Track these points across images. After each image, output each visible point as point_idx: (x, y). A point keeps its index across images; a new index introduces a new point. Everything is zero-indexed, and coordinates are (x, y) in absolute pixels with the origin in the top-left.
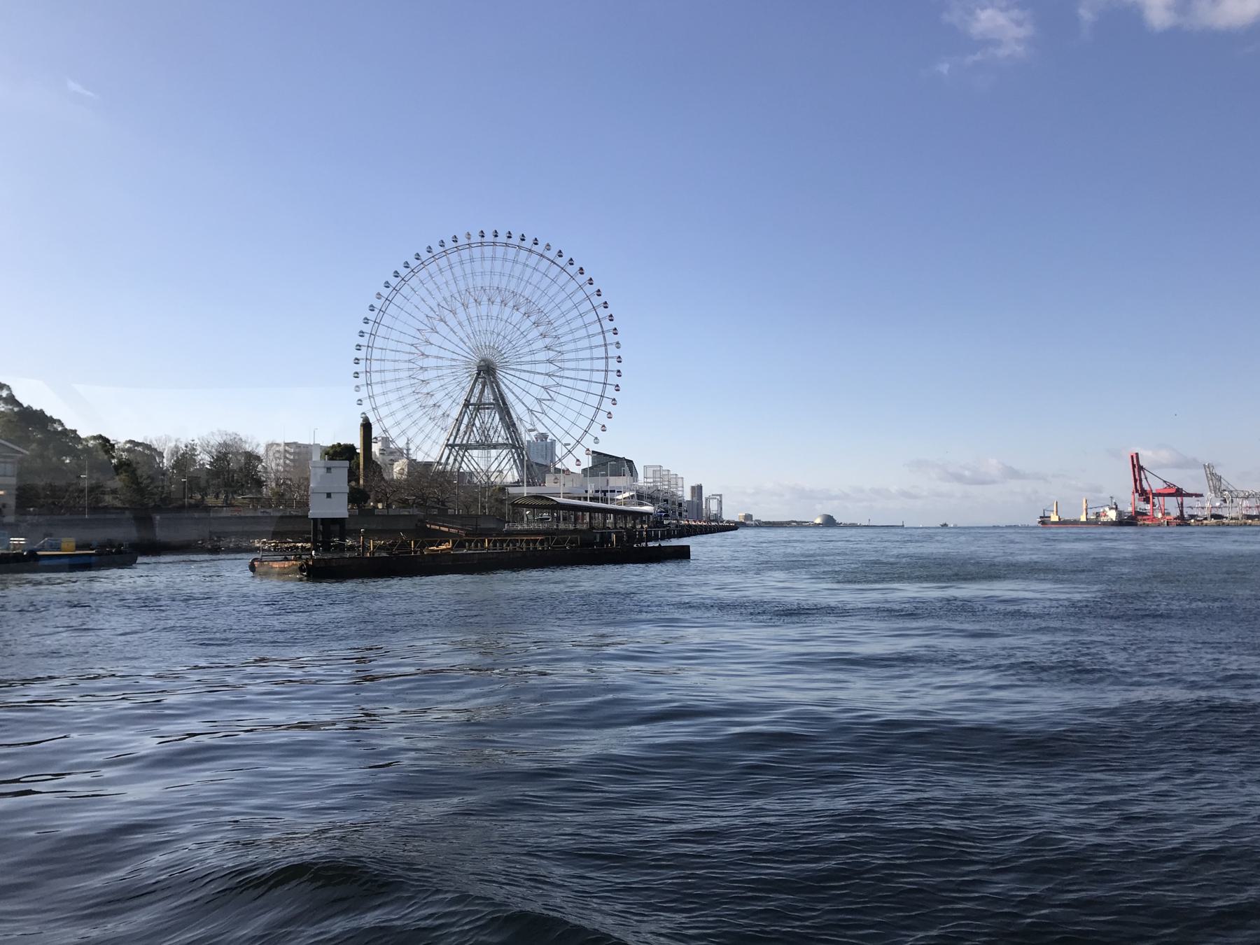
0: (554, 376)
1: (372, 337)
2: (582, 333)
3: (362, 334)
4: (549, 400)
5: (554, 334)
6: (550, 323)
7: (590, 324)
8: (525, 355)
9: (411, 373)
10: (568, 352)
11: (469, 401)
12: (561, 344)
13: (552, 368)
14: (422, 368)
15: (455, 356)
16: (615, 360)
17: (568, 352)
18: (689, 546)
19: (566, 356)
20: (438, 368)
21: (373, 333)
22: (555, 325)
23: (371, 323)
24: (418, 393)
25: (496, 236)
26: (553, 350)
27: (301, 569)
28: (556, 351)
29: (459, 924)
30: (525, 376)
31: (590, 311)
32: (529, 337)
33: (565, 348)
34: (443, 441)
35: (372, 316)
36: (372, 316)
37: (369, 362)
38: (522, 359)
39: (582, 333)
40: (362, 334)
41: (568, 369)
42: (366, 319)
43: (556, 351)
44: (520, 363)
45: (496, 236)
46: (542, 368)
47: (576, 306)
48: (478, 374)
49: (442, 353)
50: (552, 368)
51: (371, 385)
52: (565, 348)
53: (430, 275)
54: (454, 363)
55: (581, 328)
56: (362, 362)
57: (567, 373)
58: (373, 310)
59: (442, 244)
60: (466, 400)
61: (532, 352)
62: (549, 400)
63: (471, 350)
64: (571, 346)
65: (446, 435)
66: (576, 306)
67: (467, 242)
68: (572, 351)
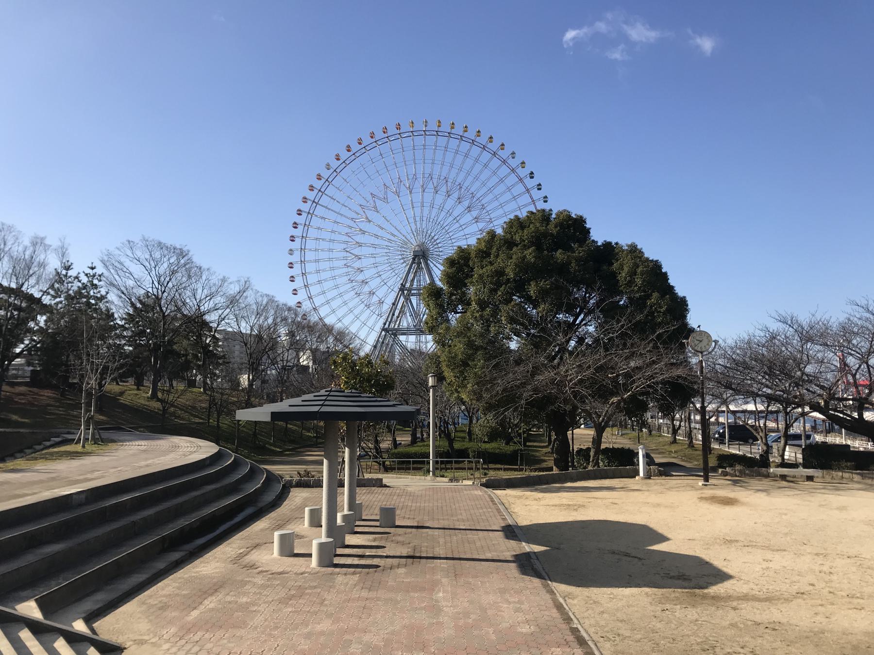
2: (508, 196)
9: (349, 231)
11: (404, 286)
15: (396, 233)
20: (374, 246)
23: (309, 203)
24: (348, 266)
27: (158, 299)
32: (462, 222)
34: (380, 325)
36: (318, 184)
37: (310, 216)
39: (508, 196)
40: (305, 200)
42: (295, 223)
45: (466, 131)
48: (414, 259)
49: (385, 225)
51: (317, 204)
53: (381, 155)
54: (392, 238)
55: (504, 192)
58: (320, 179)
59: (398, 127)
60: (402, 284)
65: (382, 321)
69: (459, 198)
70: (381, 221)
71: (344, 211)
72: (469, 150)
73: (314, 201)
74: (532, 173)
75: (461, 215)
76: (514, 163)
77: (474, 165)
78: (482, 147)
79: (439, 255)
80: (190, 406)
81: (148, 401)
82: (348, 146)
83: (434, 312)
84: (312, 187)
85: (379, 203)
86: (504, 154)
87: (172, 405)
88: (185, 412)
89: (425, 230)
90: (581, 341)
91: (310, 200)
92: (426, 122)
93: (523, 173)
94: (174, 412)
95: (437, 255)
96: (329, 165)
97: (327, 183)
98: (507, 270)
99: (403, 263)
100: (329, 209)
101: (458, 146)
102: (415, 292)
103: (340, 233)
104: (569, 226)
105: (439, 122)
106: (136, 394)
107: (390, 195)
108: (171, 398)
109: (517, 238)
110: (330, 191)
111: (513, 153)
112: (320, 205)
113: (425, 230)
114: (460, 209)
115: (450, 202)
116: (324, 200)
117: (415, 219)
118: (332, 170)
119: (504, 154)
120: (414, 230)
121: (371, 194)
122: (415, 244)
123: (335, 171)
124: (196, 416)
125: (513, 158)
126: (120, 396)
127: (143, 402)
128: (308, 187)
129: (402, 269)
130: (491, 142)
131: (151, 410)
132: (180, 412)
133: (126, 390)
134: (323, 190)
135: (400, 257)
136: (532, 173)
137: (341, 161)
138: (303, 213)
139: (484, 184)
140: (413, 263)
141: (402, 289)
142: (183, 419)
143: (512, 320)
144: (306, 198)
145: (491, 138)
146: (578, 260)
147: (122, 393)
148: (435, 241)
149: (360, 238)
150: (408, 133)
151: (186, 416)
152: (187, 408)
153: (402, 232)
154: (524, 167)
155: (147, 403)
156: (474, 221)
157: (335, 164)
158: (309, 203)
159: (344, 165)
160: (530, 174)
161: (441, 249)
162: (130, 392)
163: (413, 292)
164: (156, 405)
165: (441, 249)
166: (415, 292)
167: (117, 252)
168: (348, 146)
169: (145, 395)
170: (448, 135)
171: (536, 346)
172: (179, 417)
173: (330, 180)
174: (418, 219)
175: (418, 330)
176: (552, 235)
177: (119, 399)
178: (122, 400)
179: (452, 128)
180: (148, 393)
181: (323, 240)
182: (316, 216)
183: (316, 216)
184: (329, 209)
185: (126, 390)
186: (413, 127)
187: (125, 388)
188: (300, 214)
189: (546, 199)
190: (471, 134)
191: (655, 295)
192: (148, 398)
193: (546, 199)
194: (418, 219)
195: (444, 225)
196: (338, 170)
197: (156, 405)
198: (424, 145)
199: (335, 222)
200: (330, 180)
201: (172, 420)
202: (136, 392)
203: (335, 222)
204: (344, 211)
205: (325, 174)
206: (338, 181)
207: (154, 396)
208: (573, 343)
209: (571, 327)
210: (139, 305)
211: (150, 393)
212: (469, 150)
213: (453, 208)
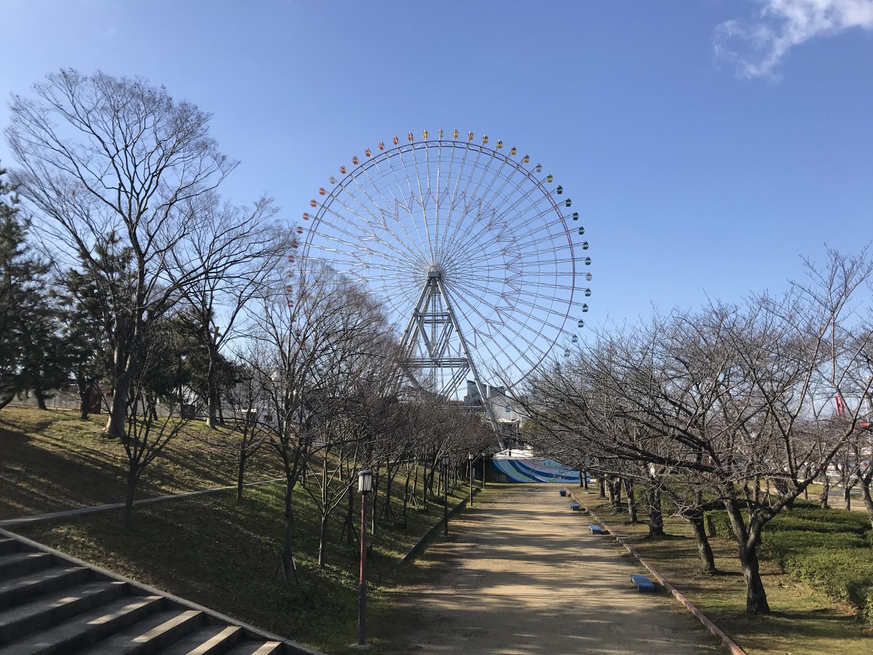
1: (323, 210)
4: (486, 335)
5: (520, 269)
6: (519, 256)
7: (564, 274)
8: (479, 278)
10: (519, 311)
12: (522, 283)
13: (495, 317)
16: (584, 278)
17: (519, 311)
19: (515, 315)
22: (524, 260)
24: (353, 273)
26: (507, 301)
31: (569, 274)
33: (519, 306)
35: (321, 199)
36: (321, 199)
37: (317, 221)
38: (472, 290)
43: (510, 304)
44: (467, 292)
46: (486, 311)
47: (554, 250)
48: (429, 281)
50: (495, 317)
51: (320, 220)
52: (519, 306)
57: (504, 331)
58: (315, 206)
60: (416, 309)
61: (488, 279)
64: (522, 318)
66: (554, 250)
69: (490, 225)
70: (392, 241)
71: (350, 228)
72: (490, 163)
74: (560, 188)
75: (481, 233)
76: (559, 199)
77: (495, 179)
78: (504, 159)
79: (455, 282)
80: (192, 453)
81: (103, 442)
82: (355, 158)
85: (389, 220)
86: (540, 176)
87: (157, 453)
88: (182, 465)
89: (445, 251)
92: (442, 132)
93: (551, 187)
94: (159, 467)
95: (452, 281)
96: (333, 179)
97: (331, 198)
99: (416, 286)
100: (333, 227)
101: (478, 158)
102: (430, 318)
103: (345, 253)
105: (457, 132)
106: (77, 427)
107: (401, 212)
108: (153, 436)
111: (539, 166)
112: (323, 222)
113: (445, 251)
114: (479, 227)
115: (468, 220)
116: (328, 217)
117: (437, 237)
118: (336, 184)
119: (529, 167)
120: (433, 248)
121: (381, 210)
122: (431, 264)
124: (206, 476)
125: (539, 171)
126: (36, 431)
127: (90, 444)
129: (417, 293)
130: (514, 154)
131: (104, 465)
132: (171, 467)
133: (56, 420)
134: (319, 217)
135: (413, 280)
136: (560, 188)
137: (347, 174)
138: (310, 218)
139: (506, 200)
140: (428, 285)
141: (417, 314)
142: (179, 484)
144: (307, 215)
145: (527, 157)
147: (42, 427)
148: (454, 265)
149: (367, 259)
150: (421, 144)
151: (184, 474)
152: (186, 458)
154: (551, 181)
155: (99, 448)
157: (340, 177)
158: (311, 220)
160: (558, 188)
161: (458, 276)
162: (65, 423)
163: (427, 318)
164: (117, 451)
165: (458, 276)
166: (430, 318)
167: (35, 97)
168: (355, 158)
169: (97, 430)
170: (466, 146)
172: (169, 479)
174: (440, 238)
175: (434, 361)
177: (33, 439)
178: (39, 441)
179: (471, 139)
180: (104, 425)
182: (319, 234)
183: (319, 234)
184: (333, 227)
185: (56, 420)
187: (56, 416)
188: (306, 219)
190: (506, 151)
192: (103, 435)
194: (440, 238)
195: (468, 251)
197: (117, 451)
198: (440, 157)
199: (341, 241)
200: (326, 205)
201: (156, 488)
202: (78, 423)
203: (341, 241)
204: (350, 228)
205: (329, 188)
206: (342, 197)
207: (116, 431)
210: (95, 256)
211: (108, 425)
212: (490, 163)
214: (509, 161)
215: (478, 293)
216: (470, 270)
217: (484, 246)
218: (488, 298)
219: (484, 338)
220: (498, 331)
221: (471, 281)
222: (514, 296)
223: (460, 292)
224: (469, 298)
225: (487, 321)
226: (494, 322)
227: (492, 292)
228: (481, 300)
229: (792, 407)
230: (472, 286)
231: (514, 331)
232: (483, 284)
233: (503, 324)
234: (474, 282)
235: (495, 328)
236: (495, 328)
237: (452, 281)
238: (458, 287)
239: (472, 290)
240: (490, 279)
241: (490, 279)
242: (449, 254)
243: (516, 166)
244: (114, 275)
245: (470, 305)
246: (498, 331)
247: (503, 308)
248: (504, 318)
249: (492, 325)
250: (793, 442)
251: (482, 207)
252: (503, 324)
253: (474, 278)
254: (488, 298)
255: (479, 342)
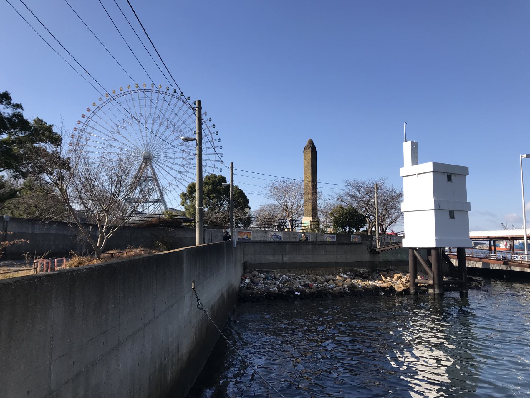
0: (182, 174)
3: (79, 122)
4: (175, 185)
13: (182, 169)
14: (114, 138)
18: (468, 168)
21: (90, 117)
25: (168, 90)
28: (188, 162)
29: (303, 342)
30: (167, 169)
36: (88, 114)
38: (167, 160)
41: (191, 173)
43: (188, 162)
44: (165, 161)
45: (168, 90)
46: (174, 173)
48: (144, 160)
50: (179, 176)
51: (85, 124)
56: (82, 124)
57: (189, 175)
62: (175, 185)
63: (144, 145)
67: (151, 88)
68: (171, 162)
69: (167, 126)
73: (85, 124)
83: (184, 200)
84: (84, 115)
89: (152, 145)
90: (224, 209)
91: (82, 123)
95: (157, 158)
98: (205, 191)
104: (221, 180)
109: (208, 182)
110: (95, 118)
113: (152, 145)
120: (145, 144)
123: (98, 107)
128: (81, 115)
140: (143, 162)
143: (206, 204)
146: (222, 189)
153: (123, 135)
156: (176, 139)
159: (104, 104)
171: (212, 210)
173: (95, 112)
176: (216, 182)
181: (91, 146)
186: (145, 87)
189: (217, 133)
191: (240, 199)
193: (217, 133)
196: (100, 107)
205: (93, 108)
208: (221, 209)
209: (221, 205)
213: (164, 132)
214: (167, 94)
215: (170, 165)
216: (164, 150)
217: (168, 137)
218: (177, 155)
219: (174, 187)
220: (186, 176)
221: (166, 159)
222: (189, 157)
223: (163, 162)
224: (167, 164)
225: (179, 172)
226: (183, 172)
227: (178, 158)
228: (173, 163)
229: (71, 205)
230: (167, 157)
231: (193, 174)
232: (172, 160)
233: (187, 172)
234: (167, 155)
235: (184, 175)
236: (184, 175)
237: (157, 158)
238: (161, 160)
239: (167, 160)
240: (175, 152)
241: (175, 152)
242: (154, 146)
243: (172, 95)
244: (163, 208)
245: (169, 167)
246: (186, 176)
247: (185, 164)
248: (187, 169)
249: (177, 180)
250: (485, 244)
251: (161, 119)
252: (187, 172)
253: (167, 153)
254: (176, 161)
255: (172, 189)
